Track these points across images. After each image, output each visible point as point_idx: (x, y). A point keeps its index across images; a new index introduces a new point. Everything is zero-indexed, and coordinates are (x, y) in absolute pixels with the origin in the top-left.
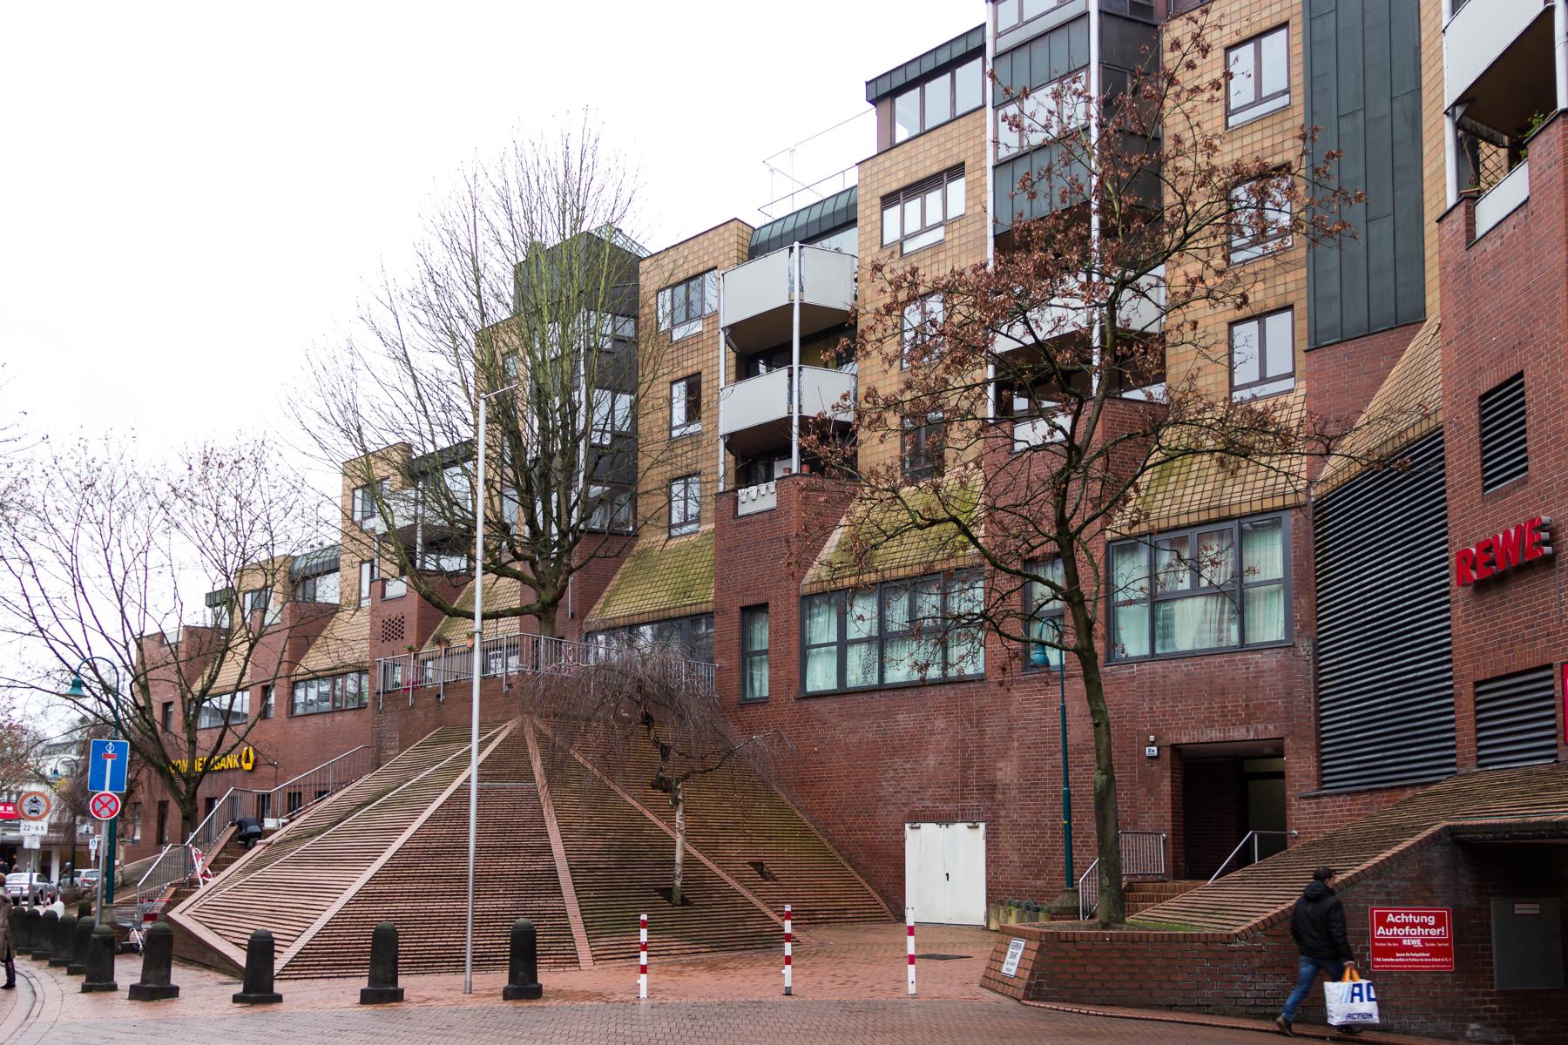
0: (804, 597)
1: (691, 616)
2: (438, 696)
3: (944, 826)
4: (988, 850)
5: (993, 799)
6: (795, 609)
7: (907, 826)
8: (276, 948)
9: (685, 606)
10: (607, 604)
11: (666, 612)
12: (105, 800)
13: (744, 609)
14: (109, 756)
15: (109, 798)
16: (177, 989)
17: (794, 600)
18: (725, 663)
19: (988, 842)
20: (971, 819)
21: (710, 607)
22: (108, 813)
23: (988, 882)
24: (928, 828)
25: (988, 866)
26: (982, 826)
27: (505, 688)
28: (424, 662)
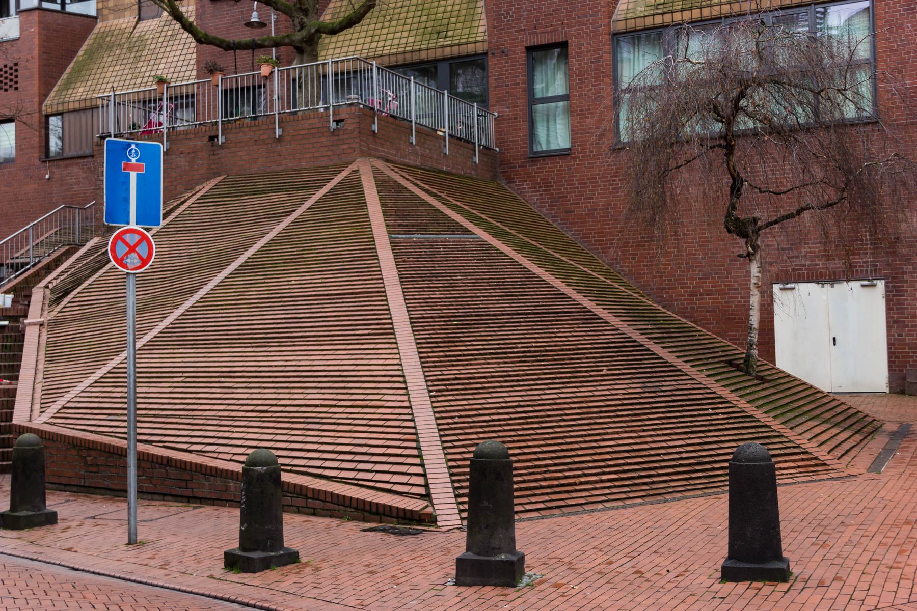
0: (615, 34)
1: (452, 58)
2: (213, 138)
3: (827, 286)
4: (889, 309)
5: (894, 253)
6: (607, 48)
7: (776, 288)
8: (777, 473)
9: (443, 47)
10: (67, 86)
11: (408, 56)
12: (132, 239)
13: (529, 49)
14: (134, 168)
15: (137, 238)
16: (55, 514)
17: (606, 38)
18: (506, 111)
19: (888, 301)
20: (868, 277)
21: (480, 48)
22: (137, 262)
23: (890, 345)
24: (806, 290)
25: (889, 327)
26: (881, 285)
27: (333, 125)
28: (47, 117)
